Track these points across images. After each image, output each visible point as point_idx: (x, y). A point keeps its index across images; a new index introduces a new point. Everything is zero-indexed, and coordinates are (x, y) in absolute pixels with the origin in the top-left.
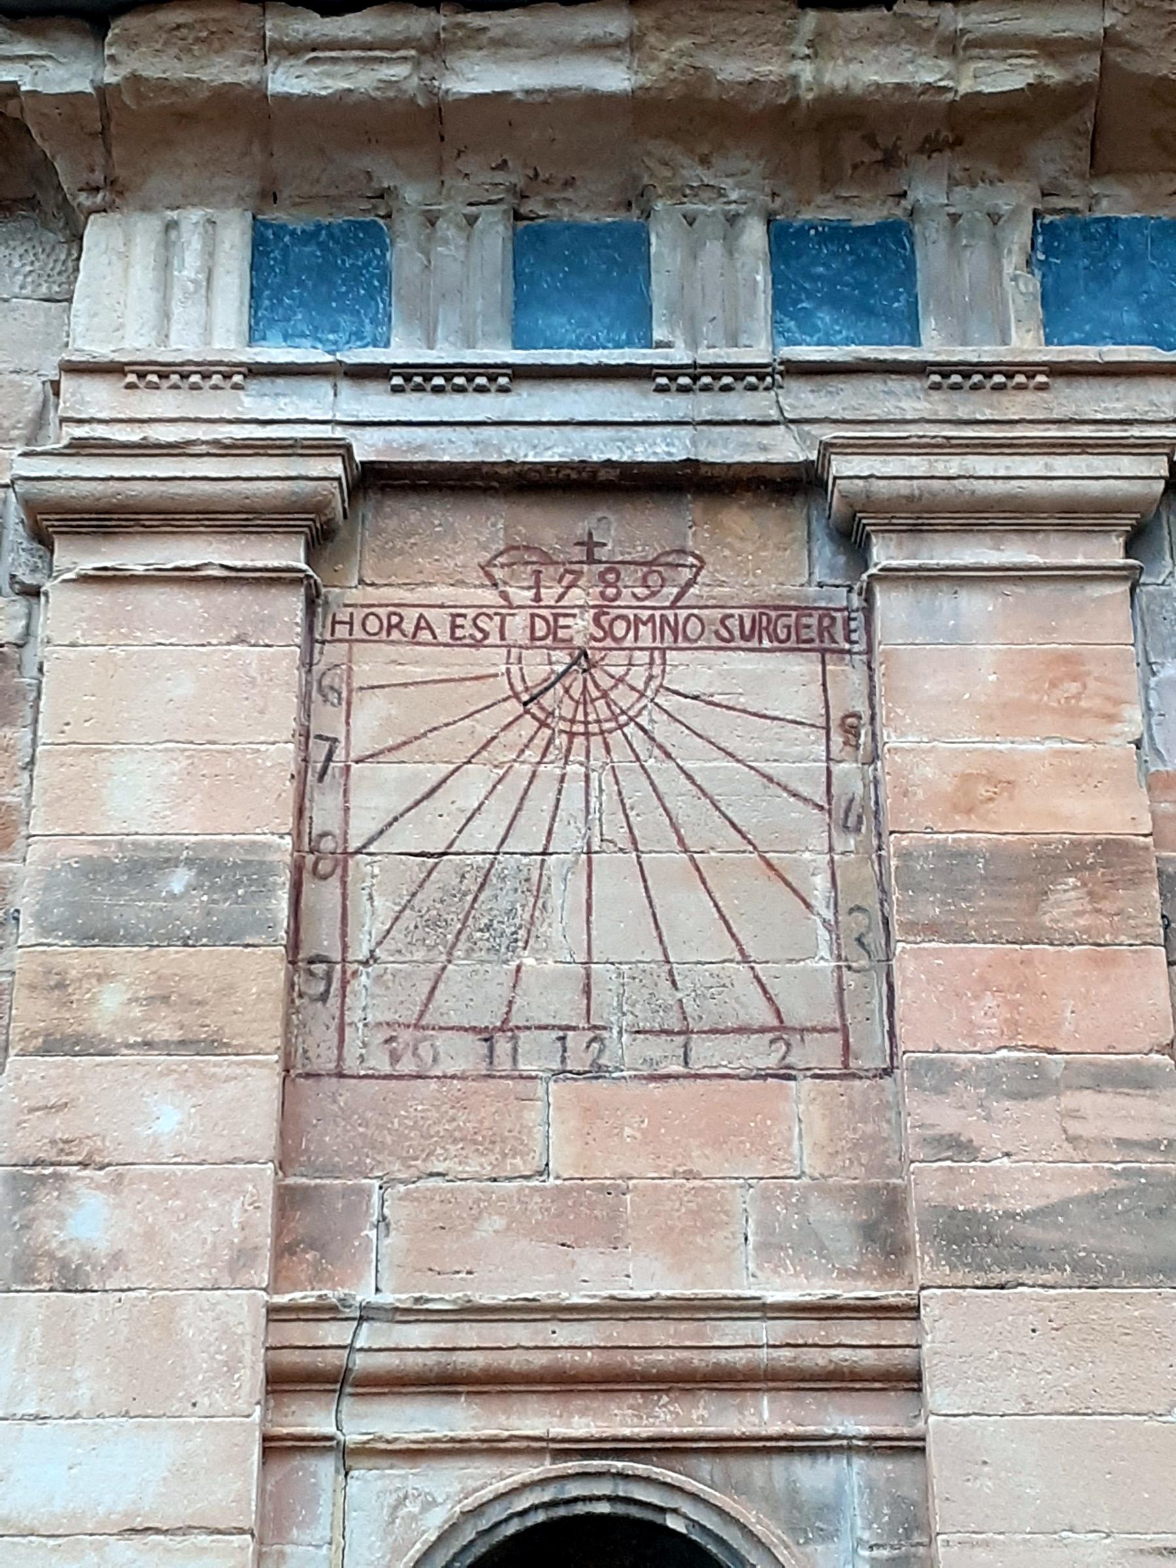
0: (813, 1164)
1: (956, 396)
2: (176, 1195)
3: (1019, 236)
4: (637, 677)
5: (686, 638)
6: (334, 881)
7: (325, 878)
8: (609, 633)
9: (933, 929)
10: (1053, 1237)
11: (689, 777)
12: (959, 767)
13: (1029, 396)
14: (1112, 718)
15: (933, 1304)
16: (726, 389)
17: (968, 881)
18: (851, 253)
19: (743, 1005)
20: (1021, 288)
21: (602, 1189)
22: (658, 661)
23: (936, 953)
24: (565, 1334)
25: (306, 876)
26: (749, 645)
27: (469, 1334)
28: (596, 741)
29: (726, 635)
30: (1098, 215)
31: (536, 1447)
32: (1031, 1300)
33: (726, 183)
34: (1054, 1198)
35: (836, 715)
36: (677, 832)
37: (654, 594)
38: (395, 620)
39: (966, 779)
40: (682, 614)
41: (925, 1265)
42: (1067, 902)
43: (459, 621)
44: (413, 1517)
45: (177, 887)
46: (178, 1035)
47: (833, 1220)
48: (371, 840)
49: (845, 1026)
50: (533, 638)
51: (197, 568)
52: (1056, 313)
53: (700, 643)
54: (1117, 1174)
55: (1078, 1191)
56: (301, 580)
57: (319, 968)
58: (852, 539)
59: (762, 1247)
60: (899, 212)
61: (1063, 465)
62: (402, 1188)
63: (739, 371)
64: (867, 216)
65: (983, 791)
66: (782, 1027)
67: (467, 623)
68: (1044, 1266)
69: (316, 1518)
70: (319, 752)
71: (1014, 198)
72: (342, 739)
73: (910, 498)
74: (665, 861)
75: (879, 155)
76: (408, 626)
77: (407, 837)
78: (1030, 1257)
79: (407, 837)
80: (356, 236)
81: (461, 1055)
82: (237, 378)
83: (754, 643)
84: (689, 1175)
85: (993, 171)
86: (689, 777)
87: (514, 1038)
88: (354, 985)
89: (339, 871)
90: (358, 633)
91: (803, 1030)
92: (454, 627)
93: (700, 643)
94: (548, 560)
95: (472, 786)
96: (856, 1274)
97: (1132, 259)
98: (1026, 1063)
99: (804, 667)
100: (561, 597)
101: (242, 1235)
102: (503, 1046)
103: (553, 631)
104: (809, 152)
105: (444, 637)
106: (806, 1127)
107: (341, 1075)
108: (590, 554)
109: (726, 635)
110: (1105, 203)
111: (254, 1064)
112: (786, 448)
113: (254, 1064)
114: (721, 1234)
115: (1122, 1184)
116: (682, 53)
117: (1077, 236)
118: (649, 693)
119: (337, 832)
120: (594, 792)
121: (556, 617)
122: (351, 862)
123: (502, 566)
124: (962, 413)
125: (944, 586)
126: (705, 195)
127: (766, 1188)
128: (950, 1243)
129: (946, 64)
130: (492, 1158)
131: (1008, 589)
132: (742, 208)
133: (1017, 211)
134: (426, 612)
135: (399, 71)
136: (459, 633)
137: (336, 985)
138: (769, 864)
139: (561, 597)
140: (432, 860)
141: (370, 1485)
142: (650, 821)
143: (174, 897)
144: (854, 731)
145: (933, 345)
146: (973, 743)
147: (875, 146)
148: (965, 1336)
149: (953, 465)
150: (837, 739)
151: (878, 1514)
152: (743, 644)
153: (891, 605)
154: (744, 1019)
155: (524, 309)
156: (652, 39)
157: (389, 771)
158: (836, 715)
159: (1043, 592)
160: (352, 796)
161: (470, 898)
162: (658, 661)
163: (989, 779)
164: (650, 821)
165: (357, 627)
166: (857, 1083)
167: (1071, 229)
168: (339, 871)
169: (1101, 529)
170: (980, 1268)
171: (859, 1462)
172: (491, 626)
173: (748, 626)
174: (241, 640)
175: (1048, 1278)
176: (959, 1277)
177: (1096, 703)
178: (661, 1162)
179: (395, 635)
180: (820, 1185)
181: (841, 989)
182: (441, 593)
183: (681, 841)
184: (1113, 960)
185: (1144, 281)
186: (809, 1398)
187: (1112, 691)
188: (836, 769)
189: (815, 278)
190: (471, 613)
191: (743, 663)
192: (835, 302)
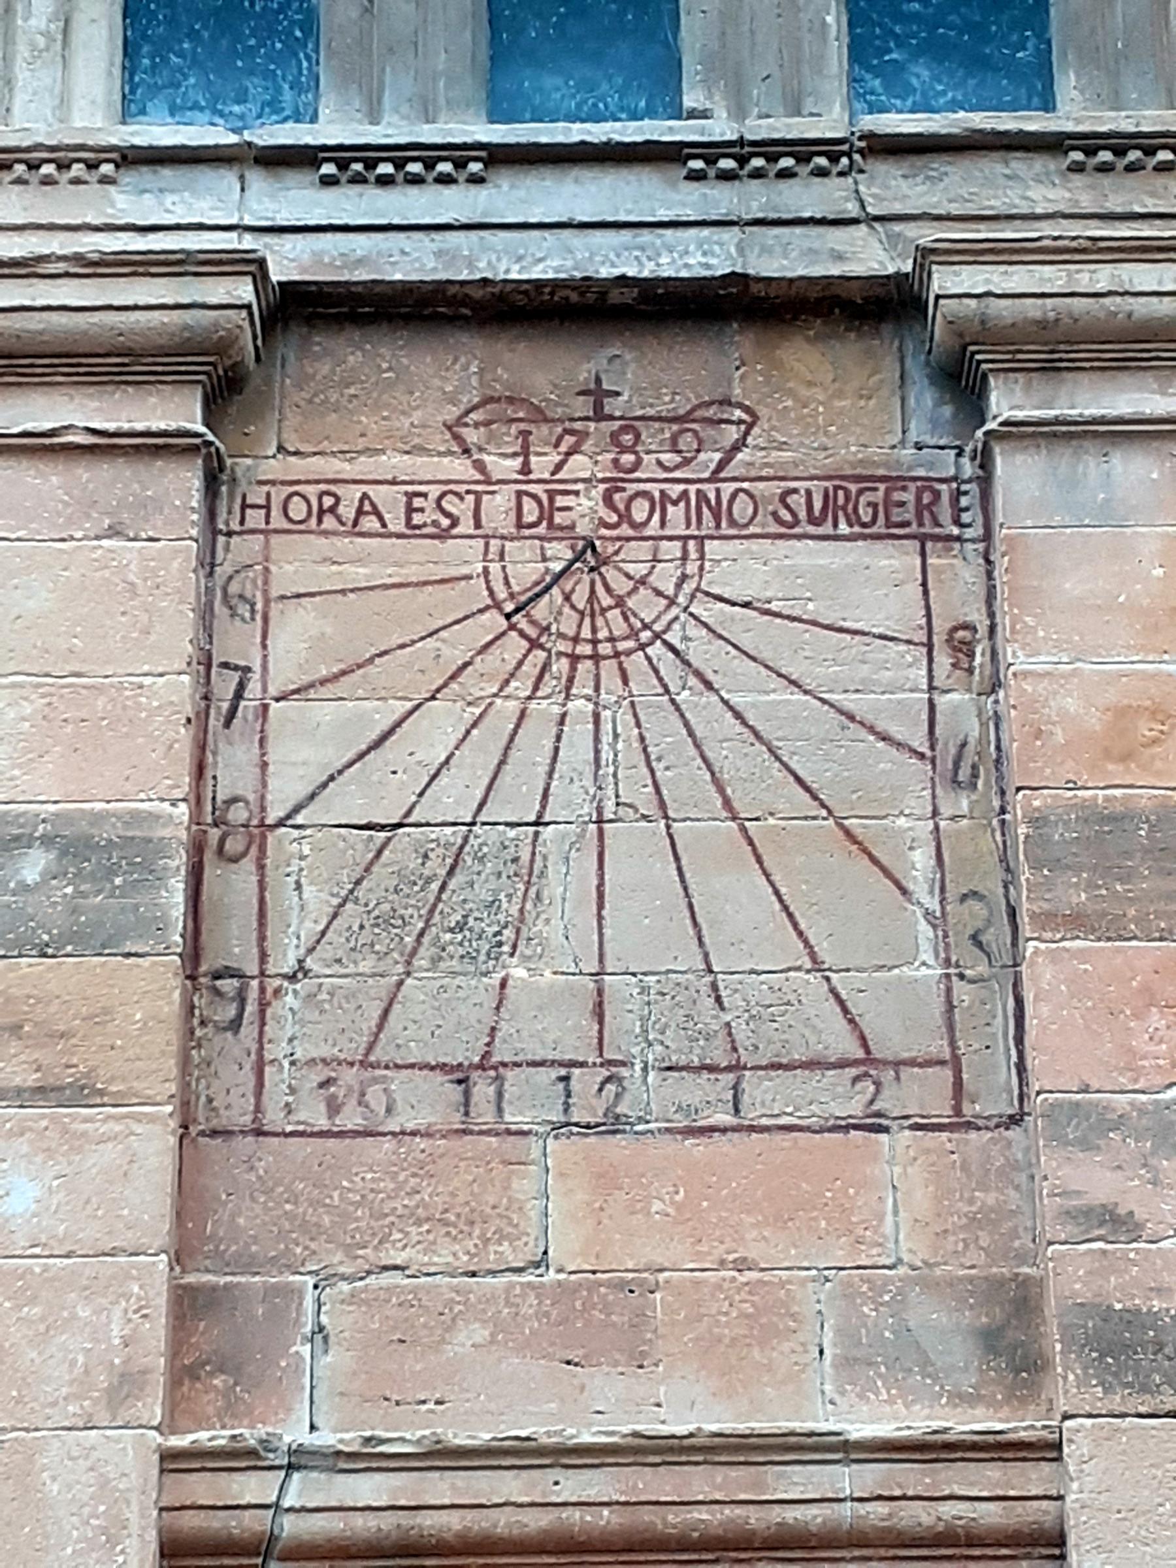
0: (912, 1248)
1: (1106, 180)
2: (33, 1301)
5: (733, 523)
6: (248, 864)
7: (235, 860)
8: (625, 517)
9: (1077, 923)
11: (738, 715)
12: (1111, 696)
16: (785, 174)
17: (1127, 854)
21: (621, 1285)
22: (693, 555)
23: (1081, 955)
24: (572, 1485)
25: (209, 856)
27: (440, 1487)
28: (609, 668)
29: (786, 516)
35: (941, 626)
36: (721, 791)
37: (687, 462)
38: (328, 502)
39: (1122, 714)
40: (728, 488)
41: (1068, 1384)
43: (417, 502)
45: (31, 875)
46: (32, 1079)
48: (297, 809)
50: (520, 525)
53: (752, 530)
56: (195, 449)
57: (228, 985)
58: (960, 382)
59: (846, 1363)
62: (345, 1287)
63: (803, 150)
65: (1146, 729)
66: (869, 1059)
67: (429, 504)
72: (257, 666)
74: (701, 830)
76: (347, 511)
77: (350, 802)
81: (423, 1103)
82: (107, 169)
83: (826, 529)
84: (741, 1265)
87: (499, 1079)
89: (254, 851)
90: (278, 521)
91: (898, 1064)
92: (410, 510)
93: (752, 530)
94: (540, 416)
95: (437, 730)
96: (972, 1400)
99: (895, 560)
100: (559, 467)
102: (483, 1090)
103: (547, 514)
105: (397, 524)
106: (902, 1195)
107: (259, 1133)
108: (598, 407)
109: (786, 516)
112: (869, 257)
114: (786, 1346)
118: (681, 599)
119: (251, 797)
120: (606, 738)
121: (551, 495)
122: (271, 839)
123: (477, 425)
124: (1115, 204)
136: (417, 519)
138: (848, 833)
139: (559, 467)
142: (684, 779)
144: (966, 648)
145: (1073, 112)
149: (1102, 277)
150: (943, 661)
152: (811, 529)
153: (1018, 475)
157: (323, 712)
158: (941, 626)
161: (435, 886)
162: (693, 555)
164: (684, 779)
165: (275, 512)
166: (973, 1135)
170: (1144, 1389)
173: (818, 505)
174: (114, 532)
179: (329, 522)
180: (925, 1280)
181: (950, 1007)
182: (393, 462)
183: (727, 803)
188: (941, 700)
190: (434, 491)
191: (808, 555)
192: (935, 50)
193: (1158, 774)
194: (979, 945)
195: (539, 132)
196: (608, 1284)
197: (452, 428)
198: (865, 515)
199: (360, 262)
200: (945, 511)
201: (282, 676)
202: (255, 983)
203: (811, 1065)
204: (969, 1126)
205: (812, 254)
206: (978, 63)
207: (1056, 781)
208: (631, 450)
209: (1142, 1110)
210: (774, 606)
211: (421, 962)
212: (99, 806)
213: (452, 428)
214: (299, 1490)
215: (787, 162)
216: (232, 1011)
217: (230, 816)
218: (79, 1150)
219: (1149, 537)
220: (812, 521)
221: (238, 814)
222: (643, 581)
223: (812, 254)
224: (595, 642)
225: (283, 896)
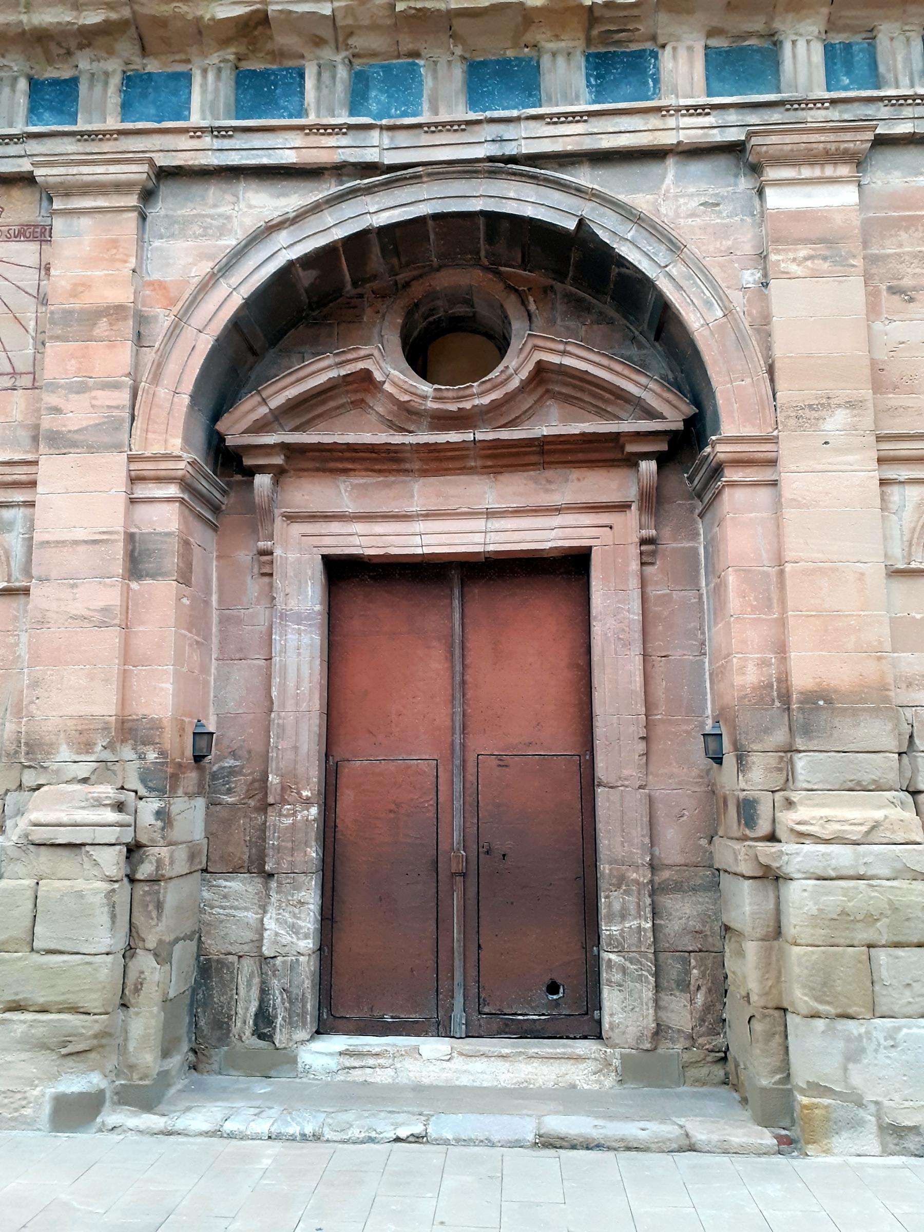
0: (19, 418)
1: (86, 143)
3: (115, 81)
9: (57, 338)
10: (81, 438)
13: (111, 143)
14: (125, 262)
15: (43, 460)
16: (7, 144)
20: (114, 99)
23: (58, 346)
33: (12, 64)
35: (43, 264)
39: (75, 285)
41: (43, 448)
42: (103, 323)
47: (24, 435)
51: (353, 193)
52: (126, 109)
55: (92, 423)
60: (77, 73)
61: (112, 169)
63: (11, 137)
64: (66, 74)
65: (80, 289)
68: (78, 447)
71: (114, 66)
73: (61, 183)
75: (65, 51)
78: (74, 444)
82: (115, 136)
85: (105, 55)
91: (21, 374)
96: (28, 452)
97: (156, 89)
98: (82, 382)
99: (34, 247)
104: (39, 50)
110: (149, 66)
112: (25, 166)
115: (106, 420)
117: (138, 80)
124: (88, 150)
125: (75, 215)
126: (6, 69)
129: (74, 13)
131: (97, 216)
133: (114, 71)
138: (16, 317)
144: (46, 269)
145: (81, 126)
146: (79, 272)
147: (62, 47)
148: (53, 471)
149: (74, 170)
150: (43, 272)
155: (474, 98)
158: (43, 264)
159: (109, 216)
169: (128, 193)
171: (22, 509)
175: (79, 451)
180: (21, 425)
181: (35, 359)
184: (114, 346)
185: (160, 96)
186: (9, 490)
188: (42, 283)
189: (43, 100)
191: (14, 246)
192: (51, 109)
198: (28, 235)
200: (47, 234)
205: (13, 166)
206: (61, 112)
207: (59, 302)
209: (67, 383)
215: (7, 141)
219: (87, 239)
223: (13, 166)
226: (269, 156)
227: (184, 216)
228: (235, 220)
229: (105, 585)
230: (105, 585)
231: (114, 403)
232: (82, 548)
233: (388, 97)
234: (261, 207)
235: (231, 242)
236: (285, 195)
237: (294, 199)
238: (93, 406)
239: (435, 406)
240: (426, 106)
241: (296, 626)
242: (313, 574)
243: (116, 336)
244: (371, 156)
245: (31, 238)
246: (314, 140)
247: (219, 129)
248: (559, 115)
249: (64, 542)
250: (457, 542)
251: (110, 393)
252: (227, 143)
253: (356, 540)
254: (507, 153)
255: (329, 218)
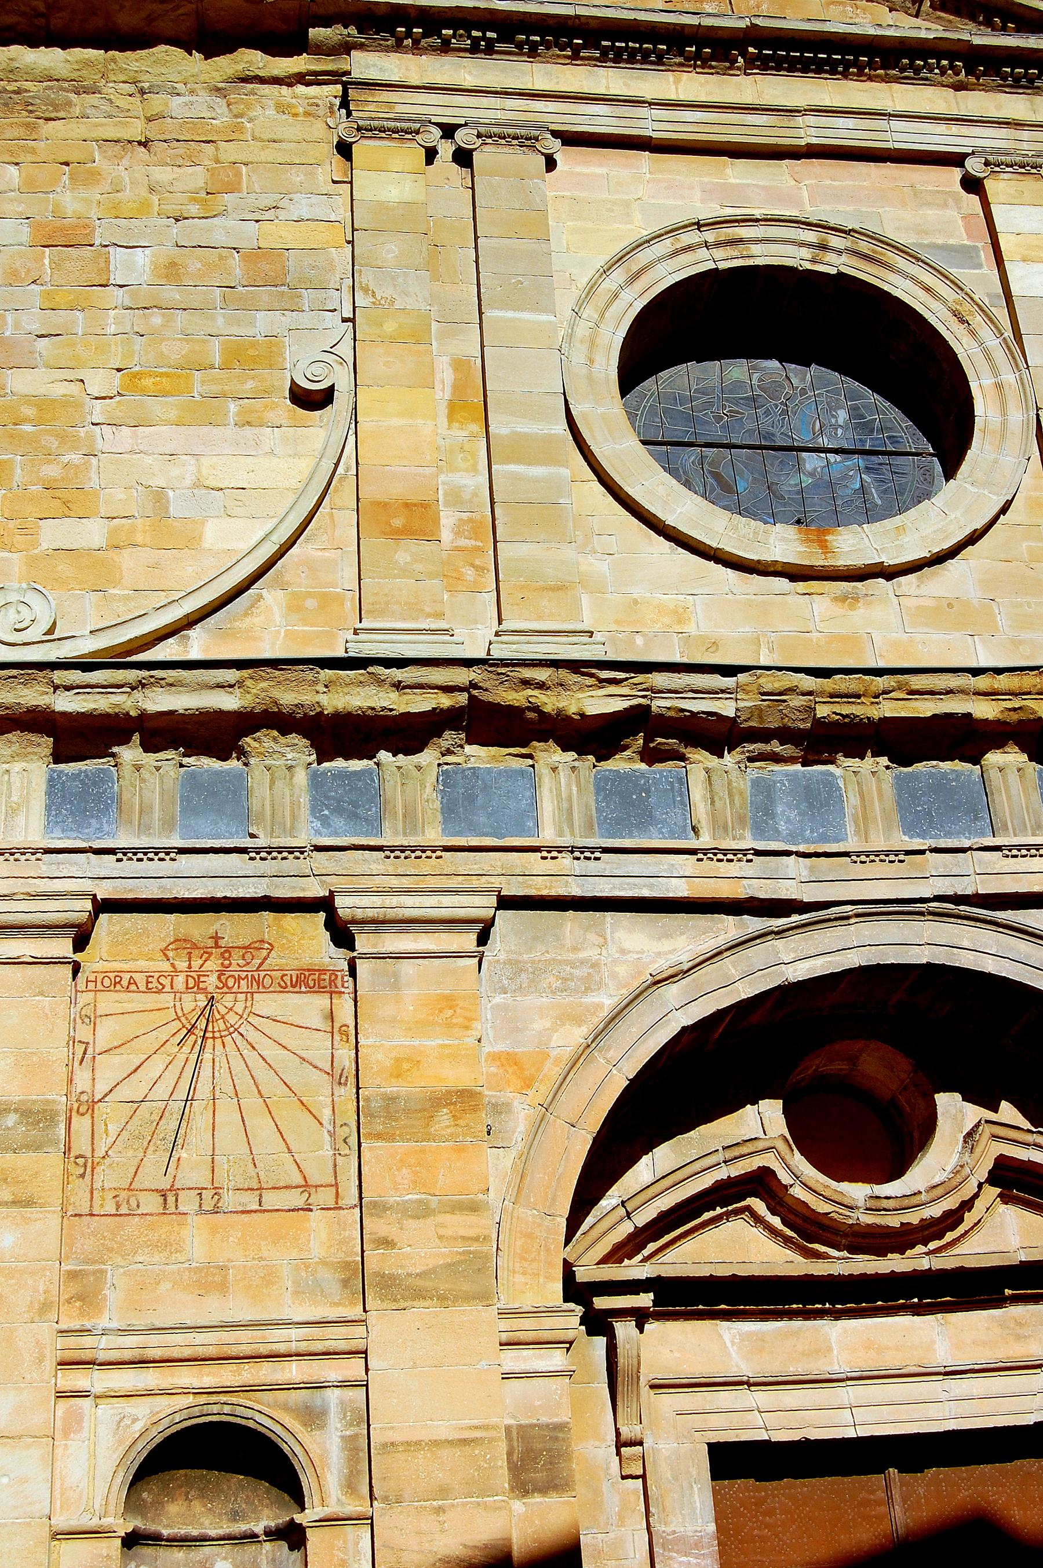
2: (12, 1278)
4: (239, 1007)
5: (264, 987)
6: (88, 1116)
7: (83, 1115)
8: (225, 985)
9: (379, 1136)
10: (429, 1284)
11: (264, 1059)
12: (393, 1054)
14: (467, 1028)
17: (397, 1112)
18: (348, 785)
19: (288, 1175)
21: (218, 1267)
22: (249, 999)
24: (200, 1338)
25: (74, 1114)
26: (295, 990)
27: (154, 1339)
28: (218, 1041)
29: (283, 984)
30: (469, 766)
31: (185, 1392)
32: (420, 1312)
34: (431, 1266)
36: (257, 1087)
37: (248, 964)
38: (118, 979)
39: (398, 1060)
40: (262, 974)
42: (444, 1117)
43: (150, 979)
44: (128, 1426)
45: (10, 1124)
46: (11, 1198)
47: (330, 1278)
48: (106, 1095)
49: (337, 1184)
50: (187, 988)
53: (271, 989)
54: (460, 1254)
56: (69, 963)
57: (80, 1161)
59: (296, 1293)
61: (447, 900)
62: (122, 1270)
65: (405, 1066)
66: (307, 1185)
67: (154, 980)
69: (82, 1428)
70: (80, 1049)
72: (91, 1043)
74: (251, 1102)
76: (125, 983)
77: (125, 1092)
78: (420, 1295)
79: (125, 1092)
80: (99, 776)
81: (151, 1203)
83: (297, 989)
84: (261, 1259)
86: (264, 1059)
87: (177, 1195)
88: (99, 1170)
89: (90, 1111)
90: (99, 987)
91: (316, 1186)
92: (148, 982)
93: (271, 989)
94: (195, 946)
95: (157, 1065)
96: (337, 1305)
98: (420, 1201)
100: (202, 966)
101: (44, 1296)
102: (171, 1199)
103: (197, 983)
105: (143, 988)
107: (92, 1215)
108: (216, 943)
109: (283, 984)
111: (48, 1212)
112: (315, 890)
113: (48, 1212)
114: (275, 1287)
115: (463, 1258)
116: (263, 690)
118: (245, 1016)
119: (89, 1091)
120: (217, 1068)
121: (199, 976)
122: (96, 1107)
123: (172, 950)
127: (297, 1265)
128: (381, 1289)
130: (165, 1254)
132: (294, 763)
133: (430, 764)
134: (134, 975)
135: (122, 698)
136: (150, 986)
137: (89, 1169)
138: (302, 1102)
139: (202, 966)
140: (137, 1105)
141: (107, 1410)
142: (244, 1083)
143: (9, 1129)
146: (402, 1041)
148: (396, 1338)
149: (394, 901)
151: (345, 1417)
152: (291, 989)
154: (289, 1182)
156: (249, 683)
157: (115, 1059)
160: (96, 1071)
161: (155, 1124)
162: (249, 999)
163: (408, 1060)
164: (244, 1083)
165: (99, 983)
166: (341, 1212)
167: (456, 774)
168: (90, 1111)
170: (395, 1300)
172: (166, 982)
173: (294, 980)
174: (41, 993)
176: (385, 1305)
177: (461, 1020)
178: (247, 1253)
179: (118, 987)
180: (324, 1263)
182: (142, 964)
183: (259, 1092)
187: (468, 1014)
190: (157, 975)
191: (293, 1000)
193: (409, 1082)
194: (346, 1143)
195: (195, 843)
196: (213, 1267)
197: (164, 951)
198: (311, 984)
199: (130, 891)
201: (101, 1045)
202: (90, 1161)
203: (286, 1187)
204: (340, 1208)
208: (228, 959)
210: (278, 1018)
211: (150, 1151)
212: (35, 1097)
213: (164, 951)
214: (104, 1342)
215: (285, 854)
216: (82, 1171)
217: (82, 1099)
218: (27, 1224)
220: (292, 986)
221: (84, 1098)
222: (231, 1009)
224: (213, 1032)
225: (100, 1128)
226: (651, 887)
227: (533, 962)
228: (604, 969)
229: (486, 1507)
230: (486, 1507)
231: (472, 1233)
232: (445, 1453)
233: (799, 814)
234: (637, 953)
235: (607, 1001)
236: (668, 936)
237: (684, 940)
238: (440, 1237)
239: (867, 1219)
240: (850, 828)
241: (684, 1559)
242: (698, 1474)
243: (465, 1135)
244: (787, 891)
245: (316, 989)
246: (708, 866)
247: (582, 849)
248: (1019, 847)
249: (418, 1443)
250: (904, 1417)
251: (464, 1217)
252: (592, 866)
253: (757, 1419)
254: (959, 893)
255: (730, 966)
